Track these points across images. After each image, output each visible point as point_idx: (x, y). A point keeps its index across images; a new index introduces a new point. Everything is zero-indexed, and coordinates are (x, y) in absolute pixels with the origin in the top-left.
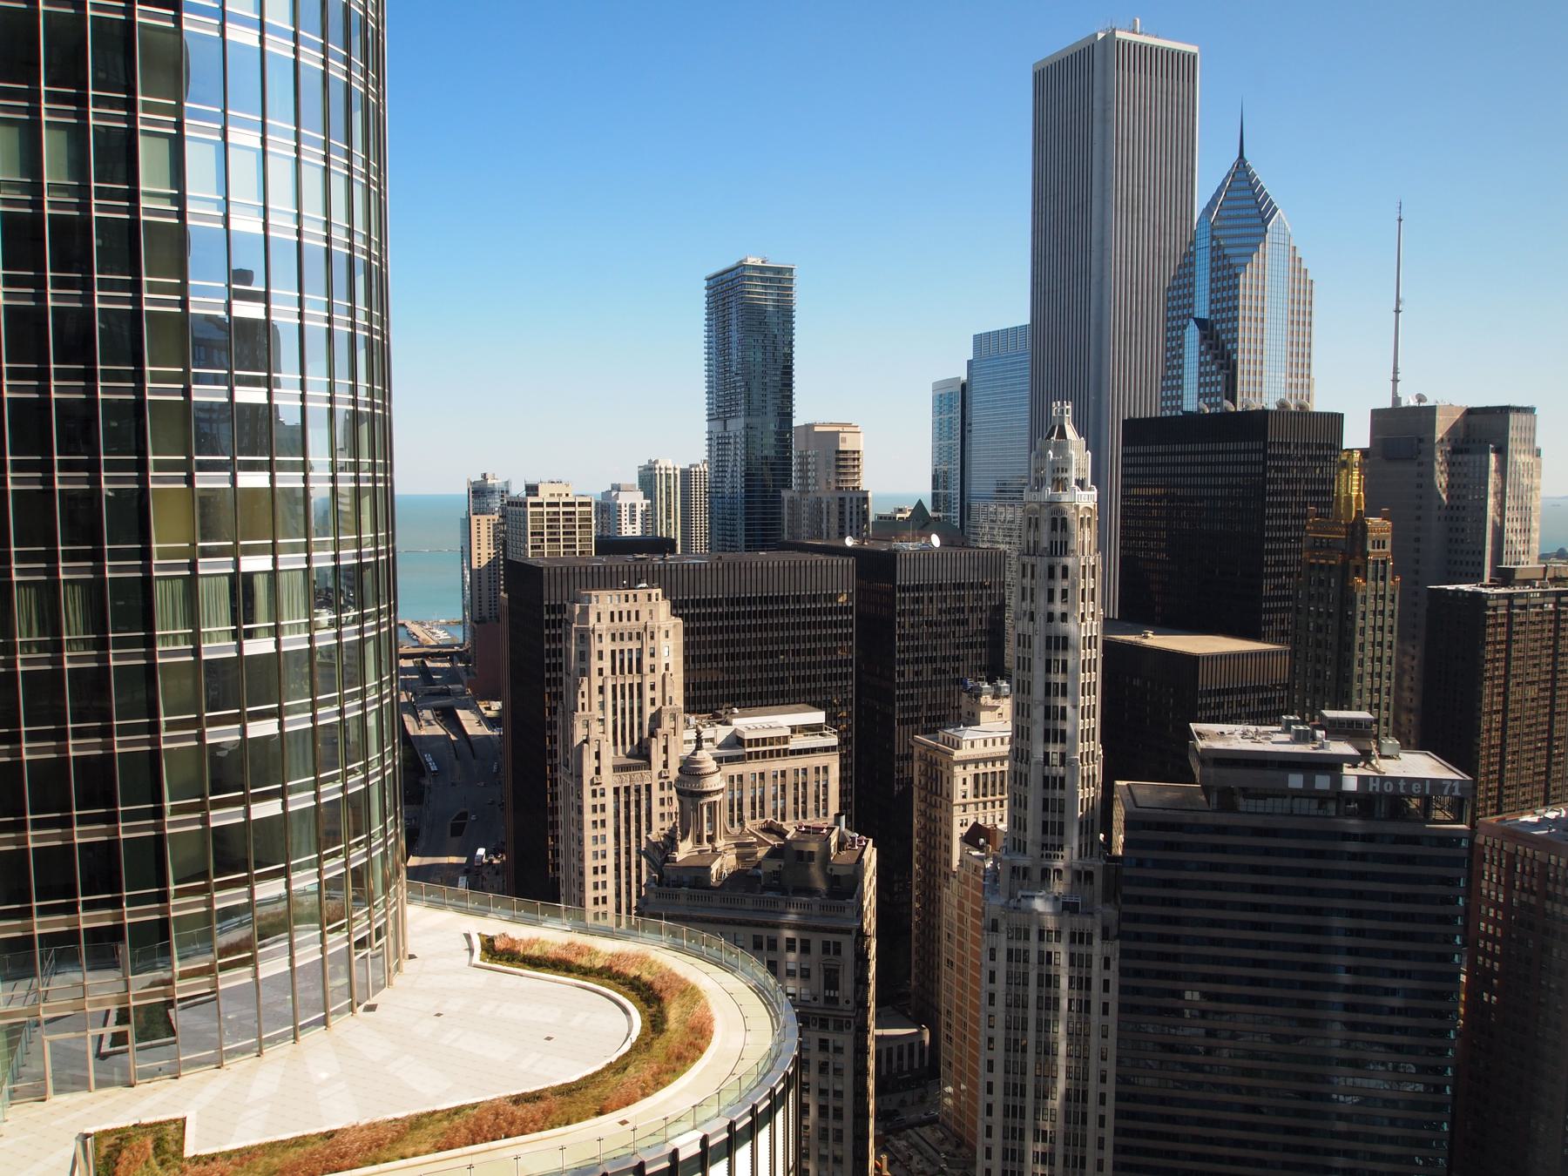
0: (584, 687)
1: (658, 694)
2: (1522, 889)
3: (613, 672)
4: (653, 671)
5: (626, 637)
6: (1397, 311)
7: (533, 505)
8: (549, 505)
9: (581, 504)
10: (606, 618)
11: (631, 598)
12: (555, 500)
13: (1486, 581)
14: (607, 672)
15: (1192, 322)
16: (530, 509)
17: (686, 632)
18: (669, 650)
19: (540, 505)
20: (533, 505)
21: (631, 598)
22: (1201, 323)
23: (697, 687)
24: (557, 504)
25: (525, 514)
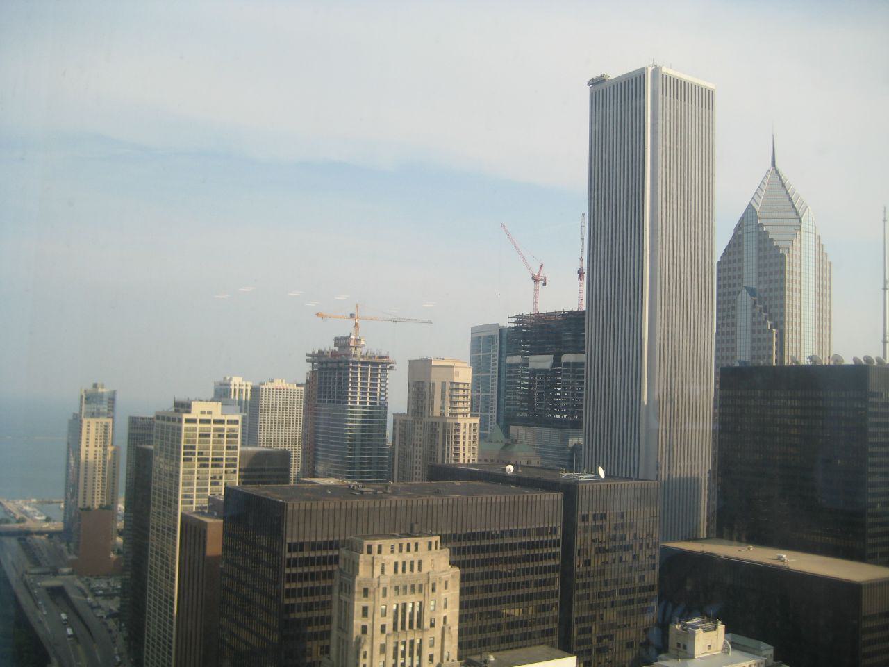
0: (366, 648)
1: (436, 651)
2: (467, 402)
3: (395, 628)
4: (432, 625)
5: (409, 589)
6: (885, 289)
7: (188, 421)
8: (202, 421)
9: (202, 421)
10: (389, 570)
11: (413, 547)
12: (206, 417)
13: (703, 533)
14: (389, 629)
15: (744, 291)
16: (184, 425)
17: (463, 578)
18: (445, 606)
19: (194, 421)
20: (188, 421)
21: (413, 547)
22: (752, 291)
23: (471, 631)
24: (208, 421)
25: (180, 429)
